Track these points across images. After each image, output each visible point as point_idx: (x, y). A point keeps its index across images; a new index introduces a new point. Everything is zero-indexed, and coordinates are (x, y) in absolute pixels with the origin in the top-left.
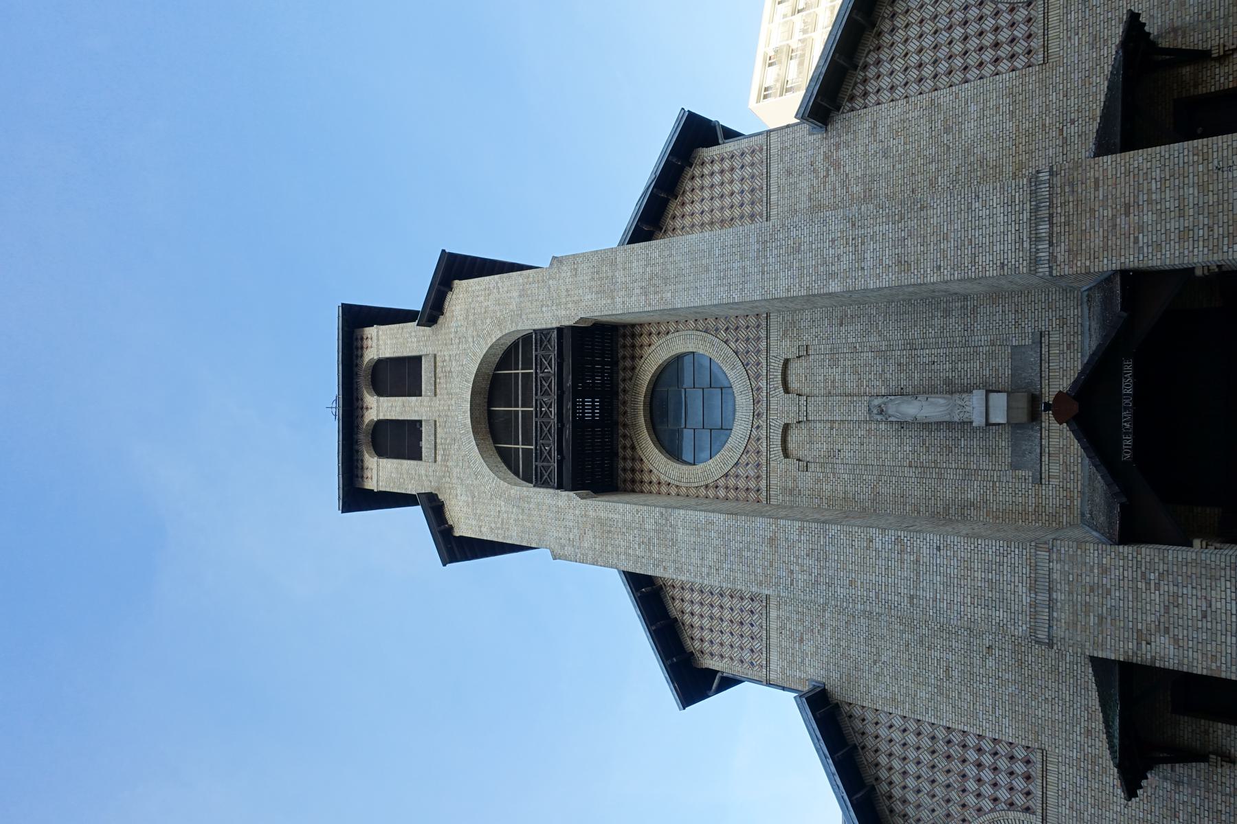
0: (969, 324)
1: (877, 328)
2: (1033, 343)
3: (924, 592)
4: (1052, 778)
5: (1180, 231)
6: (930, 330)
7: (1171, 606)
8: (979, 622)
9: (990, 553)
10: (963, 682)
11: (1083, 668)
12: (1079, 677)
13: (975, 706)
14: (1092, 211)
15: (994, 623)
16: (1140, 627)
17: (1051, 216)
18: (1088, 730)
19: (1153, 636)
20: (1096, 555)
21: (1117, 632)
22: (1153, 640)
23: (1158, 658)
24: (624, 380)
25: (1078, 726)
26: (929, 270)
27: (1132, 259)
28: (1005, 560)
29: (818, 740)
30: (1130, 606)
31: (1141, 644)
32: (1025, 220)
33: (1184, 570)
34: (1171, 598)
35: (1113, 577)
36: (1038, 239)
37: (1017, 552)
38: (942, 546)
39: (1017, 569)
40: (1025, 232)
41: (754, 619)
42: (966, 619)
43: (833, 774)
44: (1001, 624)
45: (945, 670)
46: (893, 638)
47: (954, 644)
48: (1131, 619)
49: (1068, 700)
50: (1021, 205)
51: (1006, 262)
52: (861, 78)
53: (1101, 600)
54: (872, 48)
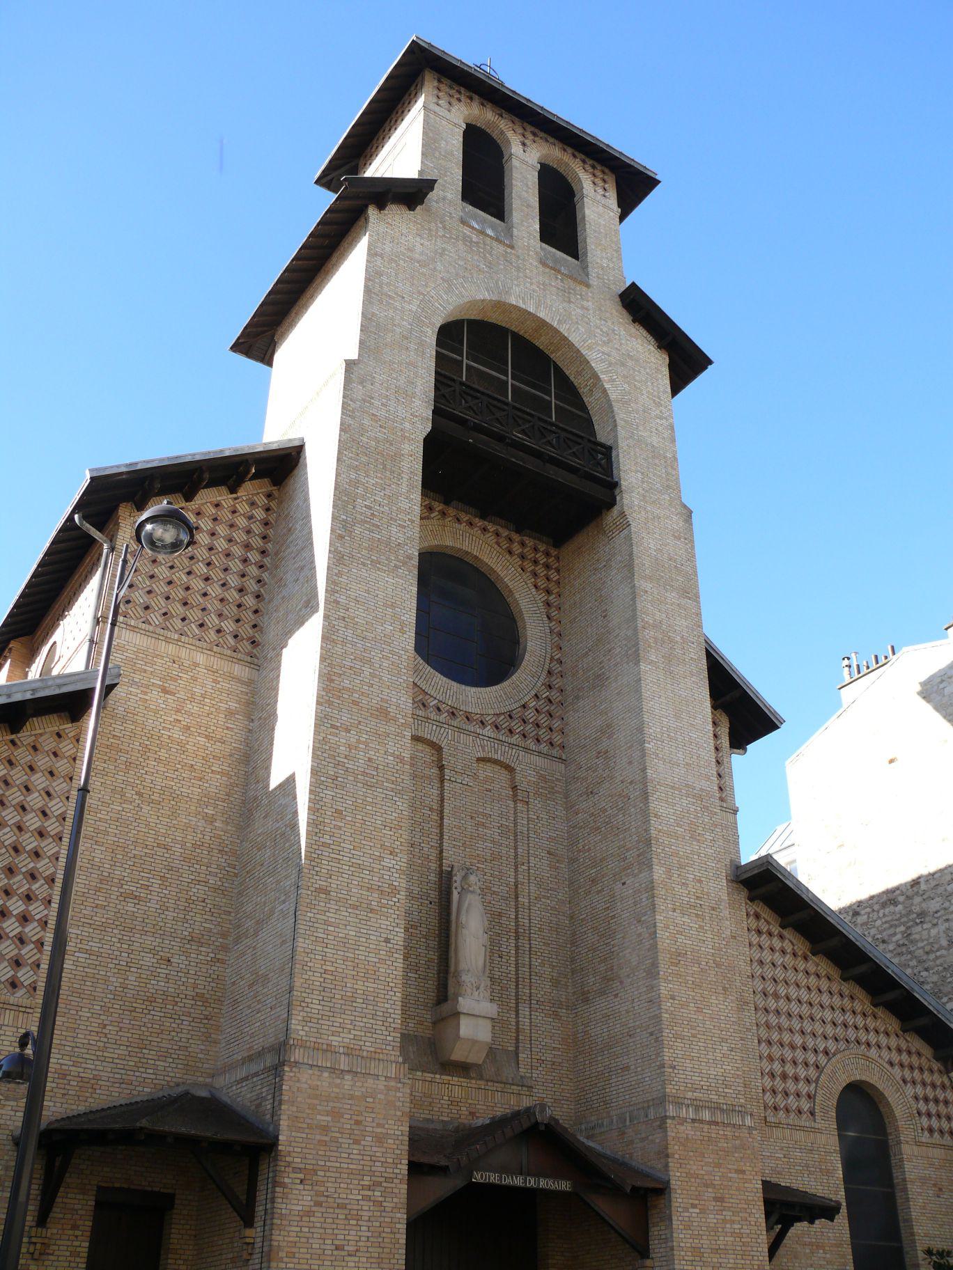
0: (543, 1007)
2: (522, 1077)
3: (334, 911)
5: (700, 1248)
6: (539, 961)
7: (346, 1212)
8: (304, 976)
9: (386, 1005)
10: (119, 915)
11: (150, 1081)
12: (137, 1074)
13: (88, 926)
14: (719, 1166)
15: (304, 995)
16: (319, 1173)
17: (716, 1123)
18: (66, 1075)
20: (396, 1133)
21: (312, 1146)
22: (306, 1187)
23: (285, 1190)
24: (497, 535)
25: (71, 1063)
26: (671, 986)
27: (679, 1200)
28: (378, 1022)
29: (59, 686)
30: (342, 1165)
31: (300, 1173)
32: (711, 1096)
33: (386, 1230)
34: (355, 1212)
35: (374, 1149)
36: (697, 1108)
37: (388, 1038)
38: (391, 946)
39: (369, 1035)
40: (701, 1095)
41: (192, 625)
42: (306, 959)
43: (9, 696)
44: (303, 1004)
45: (135, 893)
46: (173, 829)
47: (171, 915)
48: (328, 1164)
49: (105, 1054)
50: (723, 1094)
51: (676, 1071)
52: (773, 930)
53: (347, 1132)
54: (795, 948)
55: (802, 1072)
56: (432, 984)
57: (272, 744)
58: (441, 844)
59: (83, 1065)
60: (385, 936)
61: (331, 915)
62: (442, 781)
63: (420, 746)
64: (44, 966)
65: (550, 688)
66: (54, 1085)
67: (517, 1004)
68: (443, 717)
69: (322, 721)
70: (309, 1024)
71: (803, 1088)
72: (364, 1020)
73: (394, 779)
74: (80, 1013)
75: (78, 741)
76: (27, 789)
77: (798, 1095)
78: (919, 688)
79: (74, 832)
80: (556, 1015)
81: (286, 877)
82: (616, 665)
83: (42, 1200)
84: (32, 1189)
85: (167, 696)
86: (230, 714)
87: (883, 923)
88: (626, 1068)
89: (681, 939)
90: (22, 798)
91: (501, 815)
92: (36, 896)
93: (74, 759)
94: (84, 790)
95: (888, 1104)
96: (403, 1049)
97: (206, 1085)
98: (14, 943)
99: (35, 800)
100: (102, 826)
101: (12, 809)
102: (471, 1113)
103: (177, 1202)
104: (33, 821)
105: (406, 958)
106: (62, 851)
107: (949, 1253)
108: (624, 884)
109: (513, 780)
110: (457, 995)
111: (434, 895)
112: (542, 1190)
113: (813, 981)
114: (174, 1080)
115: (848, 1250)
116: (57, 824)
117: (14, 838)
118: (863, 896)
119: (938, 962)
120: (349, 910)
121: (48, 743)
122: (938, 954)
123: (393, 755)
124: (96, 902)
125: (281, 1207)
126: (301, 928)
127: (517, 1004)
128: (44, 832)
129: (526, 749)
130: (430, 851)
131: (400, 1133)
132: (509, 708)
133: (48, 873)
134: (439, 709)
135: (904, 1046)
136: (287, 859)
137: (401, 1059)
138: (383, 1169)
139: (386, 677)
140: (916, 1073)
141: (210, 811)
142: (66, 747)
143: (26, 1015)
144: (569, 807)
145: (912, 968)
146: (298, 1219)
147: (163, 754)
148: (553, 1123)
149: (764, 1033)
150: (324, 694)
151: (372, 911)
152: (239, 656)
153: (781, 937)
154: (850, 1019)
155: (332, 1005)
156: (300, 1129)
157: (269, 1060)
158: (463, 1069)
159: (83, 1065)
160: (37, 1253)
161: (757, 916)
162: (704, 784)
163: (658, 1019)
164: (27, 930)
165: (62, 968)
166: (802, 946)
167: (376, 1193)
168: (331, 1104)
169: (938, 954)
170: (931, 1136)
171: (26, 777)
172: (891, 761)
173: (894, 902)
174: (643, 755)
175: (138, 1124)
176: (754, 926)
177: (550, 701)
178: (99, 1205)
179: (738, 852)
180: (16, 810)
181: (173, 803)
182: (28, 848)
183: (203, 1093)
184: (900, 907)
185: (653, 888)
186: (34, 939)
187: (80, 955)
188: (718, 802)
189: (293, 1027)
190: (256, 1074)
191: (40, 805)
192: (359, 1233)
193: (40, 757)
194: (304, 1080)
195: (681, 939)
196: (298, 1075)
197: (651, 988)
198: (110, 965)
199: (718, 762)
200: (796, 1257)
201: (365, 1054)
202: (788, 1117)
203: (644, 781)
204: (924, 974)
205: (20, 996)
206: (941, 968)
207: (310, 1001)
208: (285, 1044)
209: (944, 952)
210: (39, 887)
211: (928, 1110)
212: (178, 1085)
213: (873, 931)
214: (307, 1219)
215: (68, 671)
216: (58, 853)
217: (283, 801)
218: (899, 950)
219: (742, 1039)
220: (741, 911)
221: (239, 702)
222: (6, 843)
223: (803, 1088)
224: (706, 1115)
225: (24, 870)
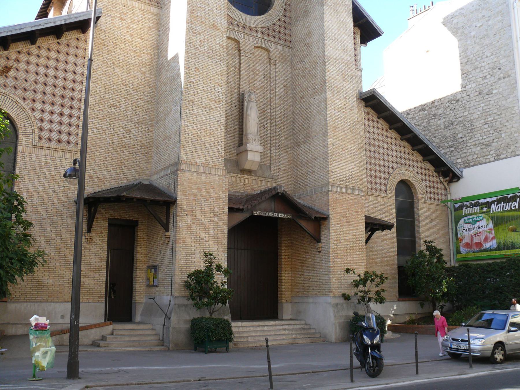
1: (282, 104)
2: (272, 175)
4: (61, 154)
7: (204, 226)
9: (218, 147)
10: (109, 113)
14: (348, 209)
15: (185, 143)
16: (194, 212)
17: (348, 194)
19: (190, 217)
21: (190, 202)
22: (189, 217)
29: (76, 18)
35: (215, 202)
36: (341, 188)
37: (219, 160)
42: (185, 129)
43: (55, 23)
44: (185, 147)
48: (197, 208)
49: (107, 169)
55: (383, 175)
56: (236, 139)
57: (168, 41)
58: (240, 82)
59: (99, 173)
60: (217, 119)
61: (195, 111)
62: (240, 56)
63: (230, 41)
64: (80, 135)
65: (285, 16)
66: (88, 181)
67: (271, 147)
68: (240, 29)
69: (190, 31)
70: (187, 155)
71: (383, 181)
72: (210, 153)
73: (220, 54)
74: (96, 153)
75: (86, 41)
76: (66, 62)
77: (381, 184)
78: (442, 20)
79: (88, 77)
80: (286, 152)
81: (176, 96)
82: (313, 7)
83: (88, 225)
84: (84, 220)
85: (122, 21)
86: (150, 28)
87: (419, 118)
88: (314, 172)
89: (337, 121)
90: (65, 66)
91: (264, 70)
92: (74, 107)
93: (85, 49)
94: (91, 60)
95: (416, 189)
96: (225, 165)
97: (148, 179)
98: (67, 126)
99: (70, 67)
100: (99, 77)
101: (61, 71)
102: (252, 189)
103: (139, 223)
104: (70, 76)
105: (226, 129)
106: (83, 88)
107: (432, 242)
108: (314, 99)
109: (269, 55)
110: (246, 143)
111: (237, 103)
112: (280, 218)
113: (389, 140)
114: (135, 178)
115: (395, 241)
116: (80, 77)
117: (63, 83)
118: (412, 107)
119: (440, 134)
120: (202, 109)
121: (73, 43)
122: (440, 131)
123: (219, 44)
124: (99, 108)
125: (179, 224)
126: (183, 116)
127: (271, 147)
128: (75, 81)
129: (275, 42)
130: (235, 85)
131: (224, 196)
132: (267, 25)
133: (78, 97)
134: (238, 25)
135: (423, 166)
136: (176, 89)
137: (224, 168)
138: (218, 210)
139: (215, 11)
140: (427, 177)
141: (144, 70)
142: (81, 44)
143: (75, 154)
144: (292, 67)
145: (429, 136)
146: (186, 228)
147: (122, 46)
148: (284, 193)
149: (368, 160)
150: (189, 18)
151: (211, 109)
152: (152, 3)
153: (378, 122)
154: (403, 155)
155: (196, 147)
156: (186, 195)
157: (172, 169)
158: (249, 172)
159: (99, 173)
160: (88, 242)
161: (368, 113)
162: (349, 58)
163: (326, 153)
164: (72, 121)
165: (87, 135)
166: (385, 126)
167: (216, 219)
168: (197, 185)
169: (440, 131)
170: (431, 200)
171: (65, 58)
172: (427, 52)
173: (424, 110)
174: (324, 45)
175: (122, 194)
176: (367, 117)
177: (285, 22)
178: (110, 225)
179: (362, 87)
180: (63, 71)
181: (128, 66)
182: (69, 87)
183: (147, 183)
184: (426, 112)
185: (326, 101)
186: (75, 124)
187: (94, 130)
188: (354, 66)
189: (181, 156)
190: (167, 175)
191: (72, 69)
192: (210, 234)
193: (70, 49)
194: (186, 176)
195: (337, 121)
196: (184, 174)
197: (324, 141)
198: (106, 134)
199: (355, 49)
200: (375, 243)
201: (210, 166)
202: (376, 192)
203: (324, 56)
204: (434, 139)
205: (71, 147)
206: (440, 137)
207: (187, 145)
208: (178, 162)
209: (442, 130)
210: (75, 103)
211: (430, 191)
212: (137, 180)
213: (414, 121)
214: (189, 228)
215: (79, 11)
216: (82, 89)
217: (174, 65)
218: (425, 129)
219: (360, 162)
220: (362, 111)
221: (153, 23)
222: (60, 86)
223: (383, 181)
224: (344, 190)
225: (68, 96)
